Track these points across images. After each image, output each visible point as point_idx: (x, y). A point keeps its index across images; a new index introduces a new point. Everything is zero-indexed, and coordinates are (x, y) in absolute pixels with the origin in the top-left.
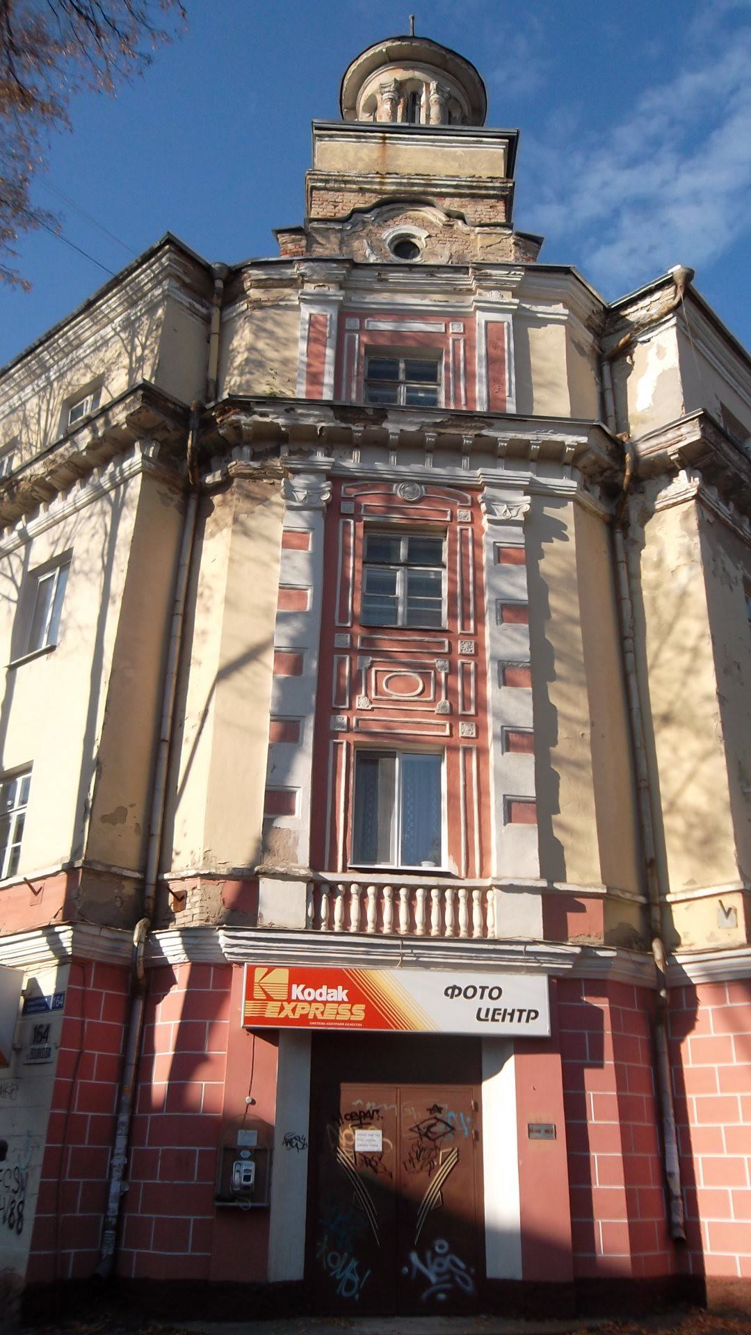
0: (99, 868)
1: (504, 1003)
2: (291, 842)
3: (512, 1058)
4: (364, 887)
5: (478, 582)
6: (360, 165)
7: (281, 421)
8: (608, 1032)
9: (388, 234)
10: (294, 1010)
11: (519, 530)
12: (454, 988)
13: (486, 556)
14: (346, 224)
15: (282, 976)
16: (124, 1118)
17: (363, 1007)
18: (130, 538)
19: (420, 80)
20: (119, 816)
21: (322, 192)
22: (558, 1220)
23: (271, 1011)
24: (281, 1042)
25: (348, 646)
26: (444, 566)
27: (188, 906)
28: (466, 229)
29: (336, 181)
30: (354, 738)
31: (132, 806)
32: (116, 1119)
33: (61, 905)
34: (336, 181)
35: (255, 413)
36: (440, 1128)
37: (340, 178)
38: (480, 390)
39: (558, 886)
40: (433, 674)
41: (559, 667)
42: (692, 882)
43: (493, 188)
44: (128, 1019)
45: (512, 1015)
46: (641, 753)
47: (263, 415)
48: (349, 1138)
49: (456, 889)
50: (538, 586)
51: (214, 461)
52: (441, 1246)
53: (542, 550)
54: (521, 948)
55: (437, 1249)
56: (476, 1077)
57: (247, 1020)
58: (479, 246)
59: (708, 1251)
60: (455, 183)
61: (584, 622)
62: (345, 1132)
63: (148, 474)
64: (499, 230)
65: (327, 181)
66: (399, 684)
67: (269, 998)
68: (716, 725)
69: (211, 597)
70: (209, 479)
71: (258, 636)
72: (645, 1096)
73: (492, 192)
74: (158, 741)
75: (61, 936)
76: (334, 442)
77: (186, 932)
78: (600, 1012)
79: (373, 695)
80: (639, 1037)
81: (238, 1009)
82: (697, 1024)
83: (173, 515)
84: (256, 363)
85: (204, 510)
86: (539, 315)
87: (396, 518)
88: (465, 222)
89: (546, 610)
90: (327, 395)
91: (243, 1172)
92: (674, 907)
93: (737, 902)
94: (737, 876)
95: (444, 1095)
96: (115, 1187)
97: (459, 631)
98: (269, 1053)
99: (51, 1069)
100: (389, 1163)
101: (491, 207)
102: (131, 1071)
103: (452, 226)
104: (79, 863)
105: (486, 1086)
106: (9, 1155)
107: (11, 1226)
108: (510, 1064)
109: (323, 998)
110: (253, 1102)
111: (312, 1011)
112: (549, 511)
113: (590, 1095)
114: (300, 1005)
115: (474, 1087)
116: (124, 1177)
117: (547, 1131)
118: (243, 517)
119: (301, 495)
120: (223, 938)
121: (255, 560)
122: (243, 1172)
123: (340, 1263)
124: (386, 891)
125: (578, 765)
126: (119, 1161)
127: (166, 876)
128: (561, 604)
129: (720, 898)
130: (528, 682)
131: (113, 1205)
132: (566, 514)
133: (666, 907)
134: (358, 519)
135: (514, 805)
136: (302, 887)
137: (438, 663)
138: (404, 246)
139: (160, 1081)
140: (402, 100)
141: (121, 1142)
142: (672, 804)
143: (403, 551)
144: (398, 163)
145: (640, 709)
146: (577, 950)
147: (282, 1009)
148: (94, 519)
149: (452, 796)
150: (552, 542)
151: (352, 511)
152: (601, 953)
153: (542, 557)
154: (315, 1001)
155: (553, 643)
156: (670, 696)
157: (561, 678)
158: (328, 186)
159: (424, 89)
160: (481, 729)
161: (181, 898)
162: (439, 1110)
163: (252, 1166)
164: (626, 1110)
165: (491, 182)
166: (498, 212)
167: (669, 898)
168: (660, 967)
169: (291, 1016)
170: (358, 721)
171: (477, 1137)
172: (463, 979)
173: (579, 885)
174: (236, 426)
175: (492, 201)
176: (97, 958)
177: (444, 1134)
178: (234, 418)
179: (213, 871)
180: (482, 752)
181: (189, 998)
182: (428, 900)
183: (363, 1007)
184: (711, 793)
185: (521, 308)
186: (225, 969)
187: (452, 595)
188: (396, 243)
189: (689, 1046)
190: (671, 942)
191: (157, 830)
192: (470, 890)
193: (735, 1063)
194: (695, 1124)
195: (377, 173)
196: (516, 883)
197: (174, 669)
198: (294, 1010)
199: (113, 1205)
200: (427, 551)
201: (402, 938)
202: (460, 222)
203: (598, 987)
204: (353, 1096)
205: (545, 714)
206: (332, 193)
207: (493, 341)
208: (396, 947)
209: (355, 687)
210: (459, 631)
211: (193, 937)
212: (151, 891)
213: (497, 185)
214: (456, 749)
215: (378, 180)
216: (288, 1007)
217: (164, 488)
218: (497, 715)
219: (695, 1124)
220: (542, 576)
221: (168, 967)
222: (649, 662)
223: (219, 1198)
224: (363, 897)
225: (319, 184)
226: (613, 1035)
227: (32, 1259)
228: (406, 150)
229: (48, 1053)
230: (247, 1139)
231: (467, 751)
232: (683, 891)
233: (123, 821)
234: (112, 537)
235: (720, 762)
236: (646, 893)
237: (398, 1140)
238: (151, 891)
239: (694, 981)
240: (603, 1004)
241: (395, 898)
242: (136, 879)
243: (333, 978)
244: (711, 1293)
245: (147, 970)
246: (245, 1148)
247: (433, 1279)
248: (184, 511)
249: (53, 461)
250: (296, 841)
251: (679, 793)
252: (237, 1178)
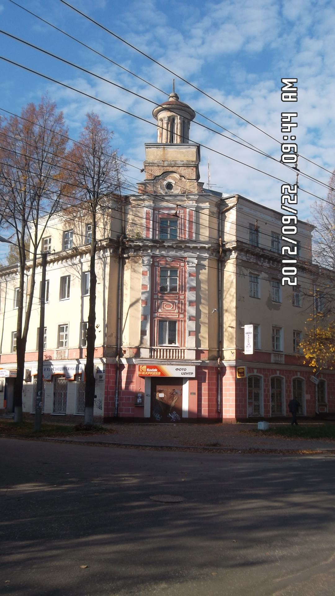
0: (109, 346)
1: (186, 371)
2: (146, 341)
3: (188, 381)
4: (160, 349)
5: (185, 282)
7: (141, 244)
8: (207, 376)
9: (165, 183)
10: (147, 373)
11: (195, 268)
12: (177, 369)
13: (187, 275)
14: (154, 180)
15: (145, 367)
16: (117, 391)
17: (160, 372)
18: (109, 273)
19: (175, 116)
21: (148, 167)
22: (195, 409)
23: (143, 373)
24: (145, 379)
25: (157, 298)
26: (178, 277)
27: (126, 353)
28: (185, 180)
29: (152, 164)
30: (158, 319)
31: (114, 333)
32: (115, 391)
33: (102, 353)
34: (152, 164)
35: (135, 242)
36: (175, 393)
37: (153, 163)
39: (199, 348)
41: (202, 301)
43: (193, 164)
44: (116, 374)
45: (188, 373)
48: (158, 395)
49: (178, 349)
50: (198, 282)
51: (126, 251)
52: (174, 412)
53: (200, 273)
54: (190, 361)
55: (174, 413)
57: (139, 375)
58: (188, 186)
59: (224, 414)
60: (182, 163)
61: (209, 290)
63: (111, 257)
65: (149, 164)
67: (143, 371)
68: (235, 314)
69: (127, 286)
70: (125, 256)
71: (138, 297)
72: (215, 387)
73: (192, 165)
74: (118, 318)
75: (104, 360)
76: (152, 248)
77: (127, 359)
79: (162, 309)
80: (214, 376)
81: (137, 373)
82: (226, 374)
83: (117, 264)
85: (124, 263)
86: (202, 207)
87: (168, 266)
88: (185, 178)
89: (200, 287)
90: (151, 237)
91: (139, 400)
92: (224, 351)
93: (235, 351)
94: (235, 346)
95: (176, 387)
96: (116, 403)
97: (181, 293)
98: (143, 381)
99: (104, 383)
100: (166, 399)
101: (192, 170)
103: (181, 179)
104: (105, 346)
106: (97, 397)
107: (100, 409)
108: (188, 382)
109: (153, 371)
110: (141, 389)
111: (151, 373)
112: (202, 262)
113: (203, 387)
114: (149, 372)
115: (181, 386)
116: (118, 401)
117: (194, 394)
119: (146, 262)
120: (134, 360)
121: (137, 278)
122: (139, 400)
123: (157, 415)
124: (165, 350)
125: (206, 323)
126: (117, 398)
127: (122, 347)
128: (204, 286)
129: (231, 350)
130: (195, 305)
131: (116, 406)
132: (206, 263)
133: (222, 351)
134: (158, 266)
135: (191, 332)
136: (148, 350)
137: (176, 301)
138: (169, 186)
139: (123, 386)
140: (170, 122)
141: (117, 395)
142: (226, 330)
143: (169, 274)
146: (201, 361)
147: (145, 373)
148: (99, 264)
149: (178, 330)
150: (202, 270)
151: (157, 265)
152: (206, 362)
153: (200, 274)
154: (151, 371)
155: (201, 295)
156: (228, 306)
157: (204, 304)
158: (150, 165)
159: (176, 118)
160: (185, 316)
161: (125, 351)
162: (175, 390)
163: (141, 399)
164: (209, 390)
165: (192, 163)
166: (194, 171)
167: (223, 349)
168: (219, 364)
169: (147, 374)
170: (159, 315)
171: (182, 394)
172: (179, 367)
173: (203, 348)
174: (131, 245)
175: (192, 167)
176: (110, 363)
177: (175, 394)
178: (130, 244)
179: (131, 347)
180: (185, 321)
181: (128, 371)
182: (173, 352)
183: (160, 372)
185: (198, 206)
187: (179, 285)
188: (167, 184)
189: (224, 378)
190: (222, 358)
191: (119, 337)
192: (181, 350)
193: (231, 382)
194: (224, 392)
195: (162, 161)
196: (190, 348)
197: (120, 302)
198: (147, 373)
199: (116, 406)
200: (174, 271)
202: (183, 178)
203: (206, 368)
204: (159, 388)
205: (198, 312)
206: (151, 167)
207: (190, 216)
208: (167, 361)
209: (158, 308)
210: (181, 293)
212: (119, 350)
213: (194, 163)
214: (179, 321)
215: (162, 163)
216: (146, 373)
217: (115, 259)
219: (224, 392)
220: (200, 279)
221: (123, 365)
223: (135, 405)
224: (160, 351)
225: (147, 165)
226: (208, 377)
227: (104, 414)
228: (170, 151)
230: (140, 395)
231: (182, 321)
232: (226, 348)
233: (112, 336)
237: (167, 395)
239: (226, 366)
240: (207, 371)
241: (167, 351)
242: (116, 348)
243: (155, 367)
244: (224, 421)
245: (119, 365)
246: (139, 396)
247: (173, 418)
248: (119, 263)
249: (87, 247)
252: (138, 401)
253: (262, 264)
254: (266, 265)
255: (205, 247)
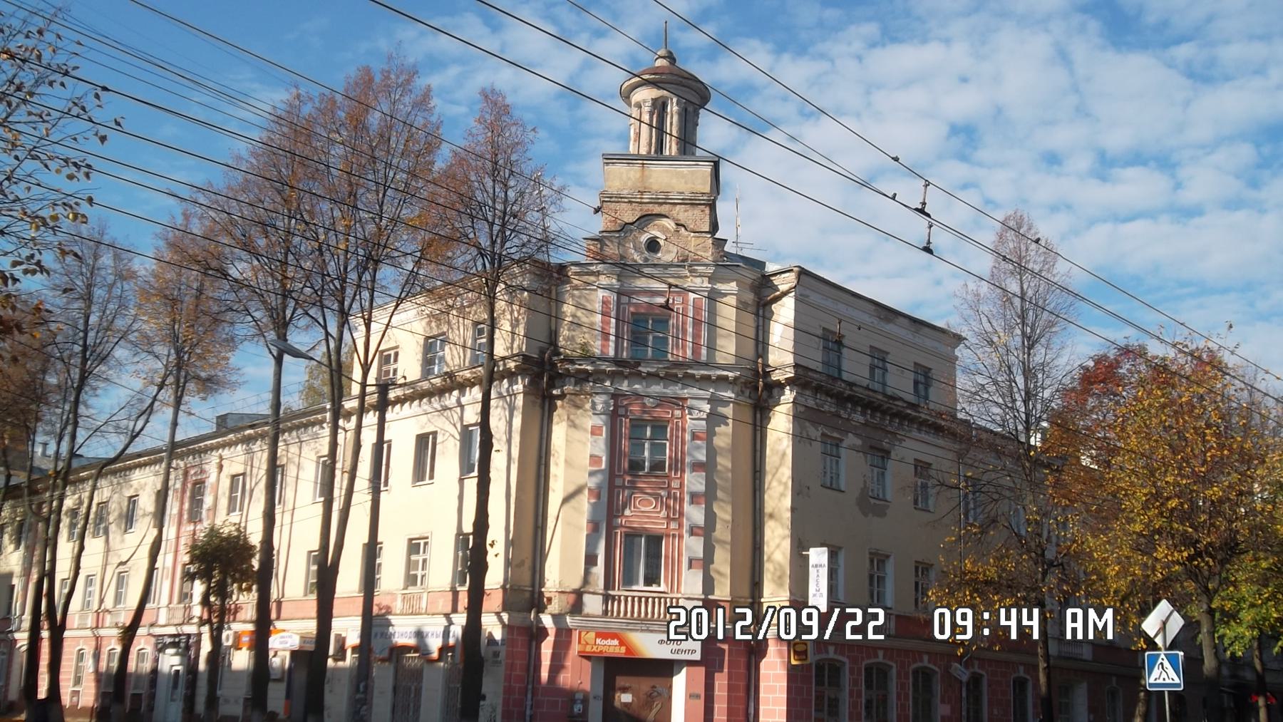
6: (630, 183)
7: (589, 368)
8: (726, 658)
9: (644, 238)
11: (704, 422)
15: (592, 635)
16: (530, 687)
20: (522, 563)
23: (588, 649)
30: (624, 530)
38: (689, 353)
39: (710, 597)
40: (668, 444)
42: (772, 594)
46: (758, 531)
47: (580, 365)
48: (619, 697)
49: (666, 598)
50: (712, 452)
56: (671, 675)
57: (579, 652)
61: (733, 470)
62: (617, 695)
63: (525, 393)
64: (704, 235)
65: (611, 197)
66: (645, 503)
67: (587, 644)
69: (558, 458)
72: (742, 684)
76: (613, 376)
77: (554, 616)
78: (724, 650)
81: (575, 648)
83: (538, 409)
84: (576, 324)
85: (553, 408)
87: (646, 417)
88: (686, 229)
89: (715, 464)
90: (611, 353)
94: (788, 594)
95: (658, 682)
96: (528, 712)
98: (587, 665)
102: (532, 669)
104: (508, 586)
105: (675, 678)
108: (684, 670)
111: (604, 649)
113: (717, 683)
116: (531, 709)
118: (572, 417)
119: (599, 407)
120: (568, 619)
122: (578, 708)
124: (636, 599)
126: (529, 703)
128: (724, 462)
132: (728, 411)
135: (693, 562)
138: (653, 245)
139: (545, 674)
141: (529, 696)
143: (648, 433)
144: (651, 180)
145: (760, 509)
149: (666, 557)
151: (624, 413)
155: (717, 481)
157: (722, 500)
160: (681, 526)
161: (550, 600)
164: (731, 688)
171: (670, 697)
178: (567, 366)
180: (681, 537)
182: (654, 603)
184: (784, 554)
185: (713, 289)
186: (569, 631)
189: (763, 664)
196: (692, 596)
200: (660, 427)
201: (642, 620)
202: (683, 229)
204: (621, 681)
205: (710, 517)
207: (697, 309)
211: (557, 618)
212: (536, 596)
216: (595, 647)
218: (688, 519)
219: (762, 695)
222: (766, 487)
229: (500, 662)
231: (674, 536)
234: (510, 423)
235: (788, 541)
236: (753, 597)
238: (536, 596)
243: (613, 636)
248: (543, 408)
249: (475, 373)
250: (598, 579)
251: (772, 553)
252: (576, 710)
253: (849, 415)
254: (858, 418)
255: (726, 378)
